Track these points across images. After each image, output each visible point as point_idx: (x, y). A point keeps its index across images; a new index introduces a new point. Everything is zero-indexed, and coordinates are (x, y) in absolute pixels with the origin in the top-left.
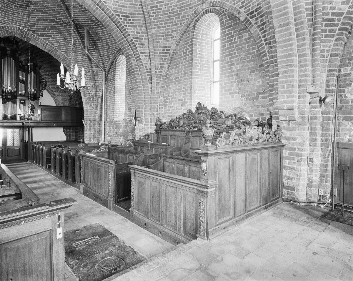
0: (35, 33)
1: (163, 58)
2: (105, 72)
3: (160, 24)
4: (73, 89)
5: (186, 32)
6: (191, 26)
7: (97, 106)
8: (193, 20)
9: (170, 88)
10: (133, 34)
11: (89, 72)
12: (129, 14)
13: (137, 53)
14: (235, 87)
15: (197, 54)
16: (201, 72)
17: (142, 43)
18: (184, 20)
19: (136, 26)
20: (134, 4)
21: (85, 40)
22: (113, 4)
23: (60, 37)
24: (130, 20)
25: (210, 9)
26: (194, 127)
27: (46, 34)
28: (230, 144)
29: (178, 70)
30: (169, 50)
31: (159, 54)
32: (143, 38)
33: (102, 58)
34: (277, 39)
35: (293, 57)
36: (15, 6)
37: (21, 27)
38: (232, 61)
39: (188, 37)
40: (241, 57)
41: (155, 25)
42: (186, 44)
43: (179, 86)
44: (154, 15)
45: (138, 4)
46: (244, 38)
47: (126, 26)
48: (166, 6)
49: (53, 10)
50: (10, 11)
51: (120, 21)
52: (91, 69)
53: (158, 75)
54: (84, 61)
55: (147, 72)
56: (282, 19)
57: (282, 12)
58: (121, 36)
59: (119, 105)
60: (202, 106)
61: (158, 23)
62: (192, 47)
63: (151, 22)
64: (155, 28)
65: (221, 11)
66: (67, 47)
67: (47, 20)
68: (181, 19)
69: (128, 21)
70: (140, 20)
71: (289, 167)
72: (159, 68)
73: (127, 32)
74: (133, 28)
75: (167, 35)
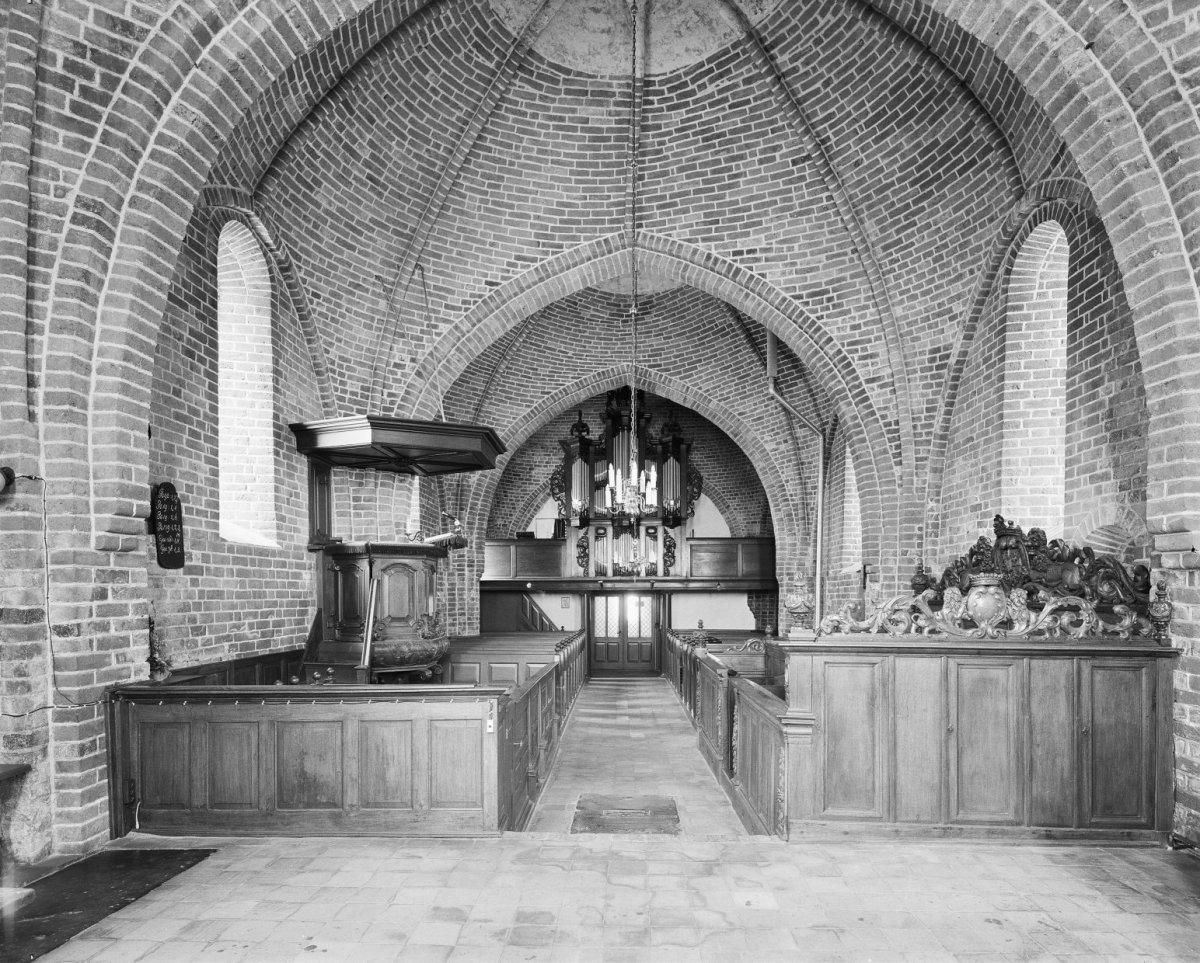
1: (933, 382)
2: (824, 436)
3: (915, 288)
4: (632, 512)
5: (988, 292)
6: (1001, 270)
7: (808, 534)
8: (1003, 252)
9: (954, 472)
10: (842, 333)
11: (786, 441)
12: (827, 283)
13: (857, 383)
14: (1104, 455)
15: (1019, 356)
16: (1035, 414)
17: (870, 352)
18: (979, 259)
19: (849, 311)
20: (838, 255)
21: (768, 356)
22: (784, 273)
23: (715, 366)
24: (830, 300)
25: (1045, 208)
28: (874, 630)
29: (972, 413)
30: (947, 356)
31: (919, 374)
32: (872, 337)
33: (815, 400)
34: (1133, 306)
35: (1178, 353)
36: (624, 321)
39: (995, 309)
40: (1121, 353)
41: (901, 294)
43: (973, 466)
44: (895, 266)
45: (849, 250)
48: (925, 233)
49: (693, 307)
52: (791, 434)
53: (921, 434)
54: (772, 414)
55: (889, 432)
56: (1133, 240)
57: (1128, 220)
58: (811, 346)
60: (1006, 524)
61: (910, 286)
64: (902, 302)
66: (730, 387)
67: (685, 333)
68: (970, 258)
70: (858, 292)
71: (1192, 729)
72: (923, 416)
74: (840, 319)
75: (939, 315)
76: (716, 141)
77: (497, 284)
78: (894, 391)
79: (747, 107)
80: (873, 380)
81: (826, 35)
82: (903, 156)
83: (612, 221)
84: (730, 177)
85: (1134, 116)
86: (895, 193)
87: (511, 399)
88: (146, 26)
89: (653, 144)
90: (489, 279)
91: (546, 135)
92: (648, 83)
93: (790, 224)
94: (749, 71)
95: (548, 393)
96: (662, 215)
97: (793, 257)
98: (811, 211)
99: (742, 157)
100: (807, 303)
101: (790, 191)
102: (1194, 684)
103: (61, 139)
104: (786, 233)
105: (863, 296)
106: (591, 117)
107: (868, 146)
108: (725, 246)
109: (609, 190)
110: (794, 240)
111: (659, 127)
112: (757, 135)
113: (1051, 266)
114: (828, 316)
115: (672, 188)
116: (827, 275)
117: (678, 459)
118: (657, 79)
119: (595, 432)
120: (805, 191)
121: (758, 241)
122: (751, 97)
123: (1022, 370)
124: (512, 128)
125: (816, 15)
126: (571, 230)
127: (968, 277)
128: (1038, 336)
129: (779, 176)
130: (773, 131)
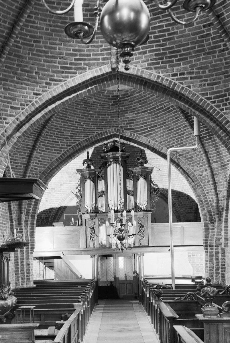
0: (135, 132)
27: (147, 128)
50: (107, 112)
51: (213, 105)
67: (147, 111)
69: (225, 102)
73: (225, 117)
77: (40, 94)
83: (104, 59)
84: (169, 35)
87: (49, 149)
90: (35, 92)
93: (203, 59)
95: (70, 146)
98: (215, 52)
100: (214, 102)
104: (201, 64)
106: (90, 3)
110: (207, 67)
116: (225, 86)
117: (145, 179)
120: (211, 41)
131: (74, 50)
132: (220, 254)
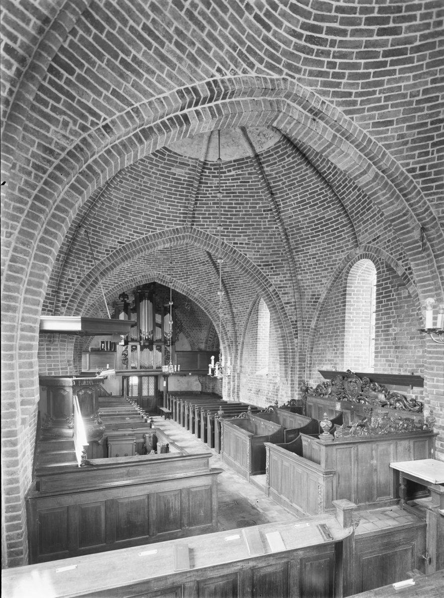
3: (307, 269)
11: (229, 314)
12: (271, 262)
18: (335, 264)
22: (254, 255)
24: (272, 268)
26: (344, 397)
30: (319, 298)
31: (306, 303)
32: (288, 286)
37: (160, 273)
38: (390, 322)
41: (301, 270)
42: (339, 292)
46: (403, 296)
47: (268, 275)
48: (314, 249)
55: (293, 325)
59: (261, 355)
62: (345, 298)
63: (296, 268)
64: (301, 274)
65: (378, 259)
68: (331, 263)
70: (283, 267)
74: (276, 277)
76: (232, 195)
77: (123, 243)
78: (296, 309)
79: (248, 184)
80: (287, 303)
81: (287, 165)
82: (310, 219)
84: (236, 211)
85: (433, 254)
86: (304, 232)
88: (60, 152)
89: (203, 190)
90: (119, 240)
91: (155, 178)
92: (205, 164)
93: (259, 235)
94: (251, 170)
95: (117, 283)
96: (204, 221)
97: (259, 248)
99: (242, 204)
100: (263, 269)
101: (260, 221)
102: (442, 445)
103: (12, 207)
105: (285, 269)
107: (296, 211)
108: (230, 240)
109: (181, 206)
110: (260, 242)
111: (207, 183)
112: (250, 196)
113: (362, 273)
114: (271, 275)
115: (210, 211)
118: (209, 163)
119: (131, 300)
120: (267, 223)
121: (245, 240)
122: (250, 180)
123: (352, 311)
124: (140, 172)
125: (285, 156)
126: (161, 222)
127: (330, 270)
128: (357, 298)
129: (257, 215)
130: (257, 196)
131: (157, 209)
132: (236, 378)
